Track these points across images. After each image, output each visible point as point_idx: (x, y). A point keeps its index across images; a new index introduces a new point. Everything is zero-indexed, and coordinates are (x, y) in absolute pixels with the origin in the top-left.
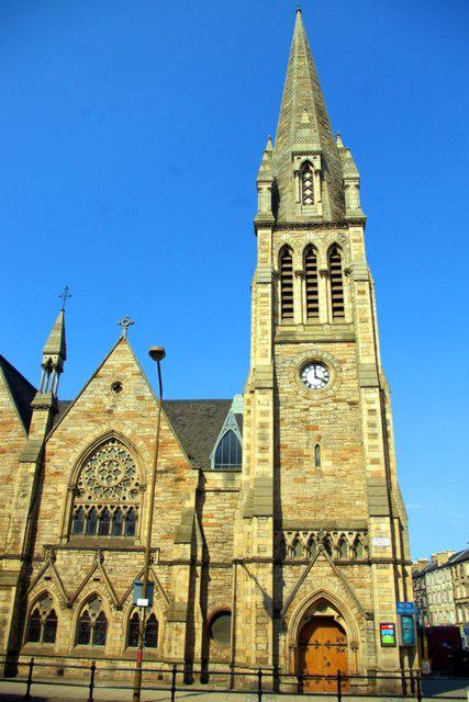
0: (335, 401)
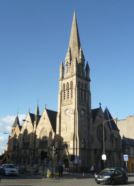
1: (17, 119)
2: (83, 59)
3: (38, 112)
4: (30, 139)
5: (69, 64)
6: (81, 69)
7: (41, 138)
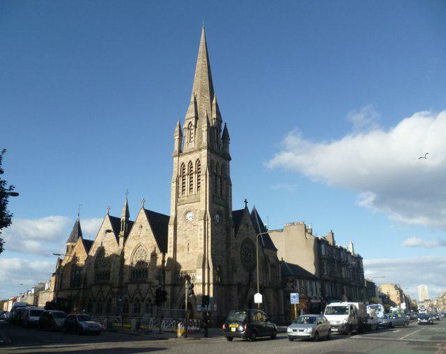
1: (77, 228)
2: (219, 119)
3: (127, 215)
4: (110, 266)
5: (192, 127)
7: (135, 263)
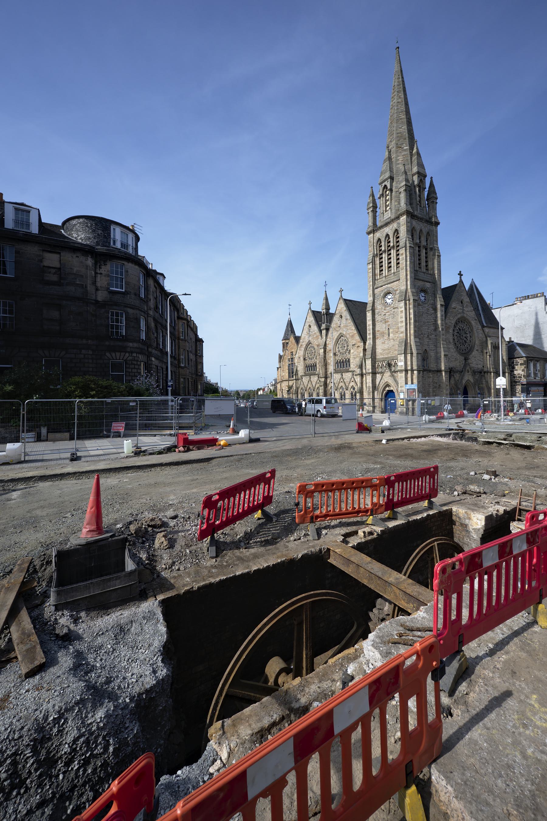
0: (394, 309)
5: (388, 192)
6: (418, 199)
